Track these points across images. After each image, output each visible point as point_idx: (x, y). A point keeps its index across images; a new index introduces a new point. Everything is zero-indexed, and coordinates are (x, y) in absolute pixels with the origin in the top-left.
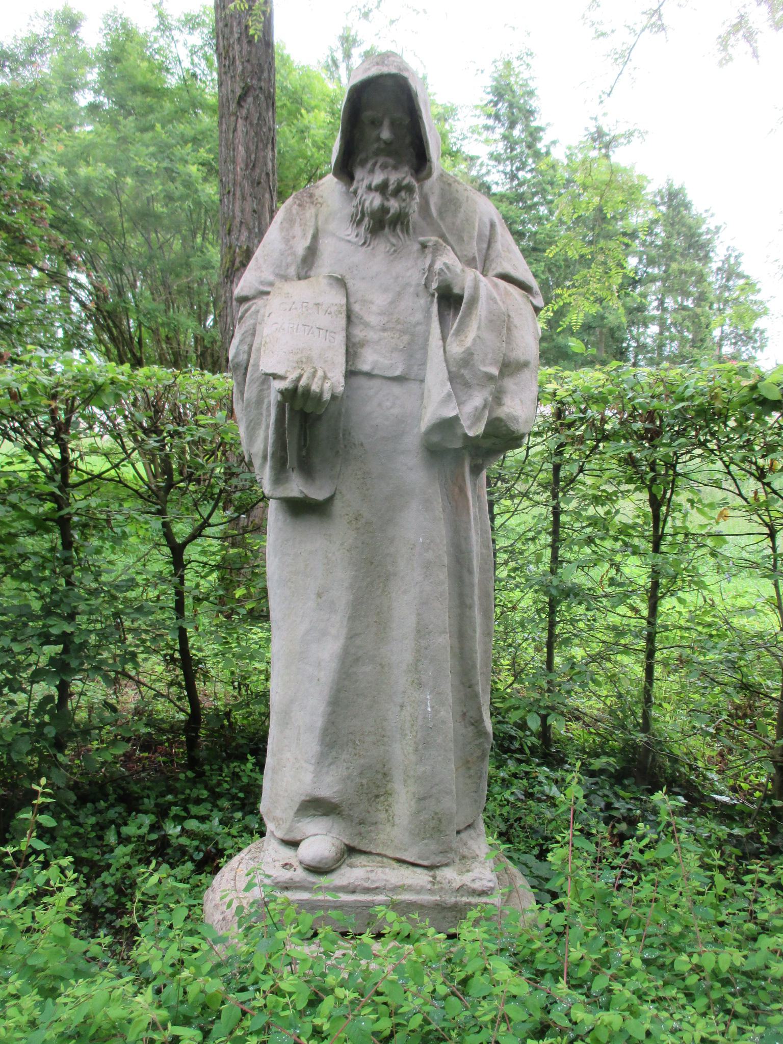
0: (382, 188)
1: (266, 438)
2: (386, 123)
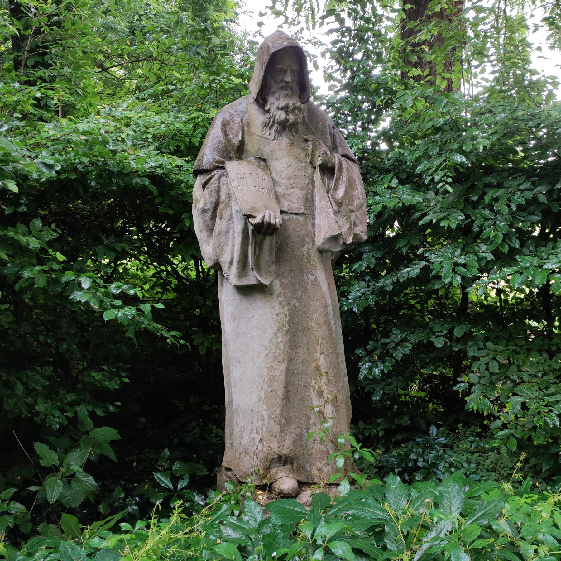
0: (285, 109)
1: (233, 252)
2: (289, 72)
